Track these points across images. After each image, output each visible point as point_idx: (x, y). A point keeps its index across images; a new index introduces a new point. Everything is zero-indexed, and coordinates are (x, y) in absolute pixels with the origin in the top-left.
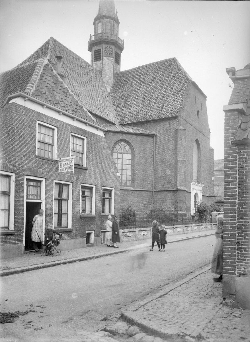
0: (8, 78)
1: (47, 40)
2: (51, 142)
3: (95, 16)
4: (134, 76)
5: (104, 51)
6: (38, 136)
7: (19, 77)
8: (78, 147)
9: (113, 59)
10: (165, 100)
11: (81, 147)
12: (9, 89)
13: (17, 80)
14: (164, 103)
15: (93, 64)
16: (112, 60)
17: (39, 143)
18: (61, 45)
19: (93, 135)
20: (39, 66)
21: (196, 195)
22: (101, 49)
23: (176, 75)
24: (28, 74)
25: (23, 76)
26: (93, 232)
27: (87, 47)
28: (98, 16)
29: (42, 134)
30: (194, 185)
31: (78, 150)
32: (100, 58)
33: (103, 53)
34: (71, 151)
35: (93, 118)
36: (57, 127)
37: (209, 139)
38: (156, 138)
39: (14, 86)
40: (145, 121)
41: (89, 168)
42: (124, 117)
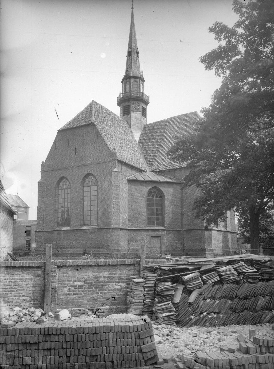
22: (129, 105)
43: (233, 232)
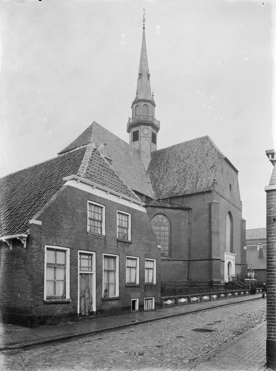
0: (60, 162)
1: (90, 124)
2: (100, 219)
3: (133, 100)
4: (169, 154)
5: (141, 132)
6: (89, 215)
7: (70, 161)
8: (124, 222)
9: (150, 139)
10: (199, 175)
11: (126, 223)
12: (63, 173)
13: (69, 164)
14: (198, 178)
15: (132, 145)
16: (149, 140)
17: (90, 220)
18: (103, 128)
19: (135, 211)
20: (88, 151)
21: (229, 263)
22: (138, 130)
23: (209, 152)
24: (78, 158)
25: (74, 160)
26: (138, 299)
27: (126, 128)
28: (135, 100)
29: (92, 212)
30: (227, 255)
31: (124, 226)
32: (138, 138)
33: (141, 134)
34: (117, 227)
35: (136, 196)
36: (105, 206)
37: (241, 211)
38: (191, 211)
39: (67, 169)
40: (181, 196)
41: (133, 241)
42: (161, 192)
43: (68, 339)
